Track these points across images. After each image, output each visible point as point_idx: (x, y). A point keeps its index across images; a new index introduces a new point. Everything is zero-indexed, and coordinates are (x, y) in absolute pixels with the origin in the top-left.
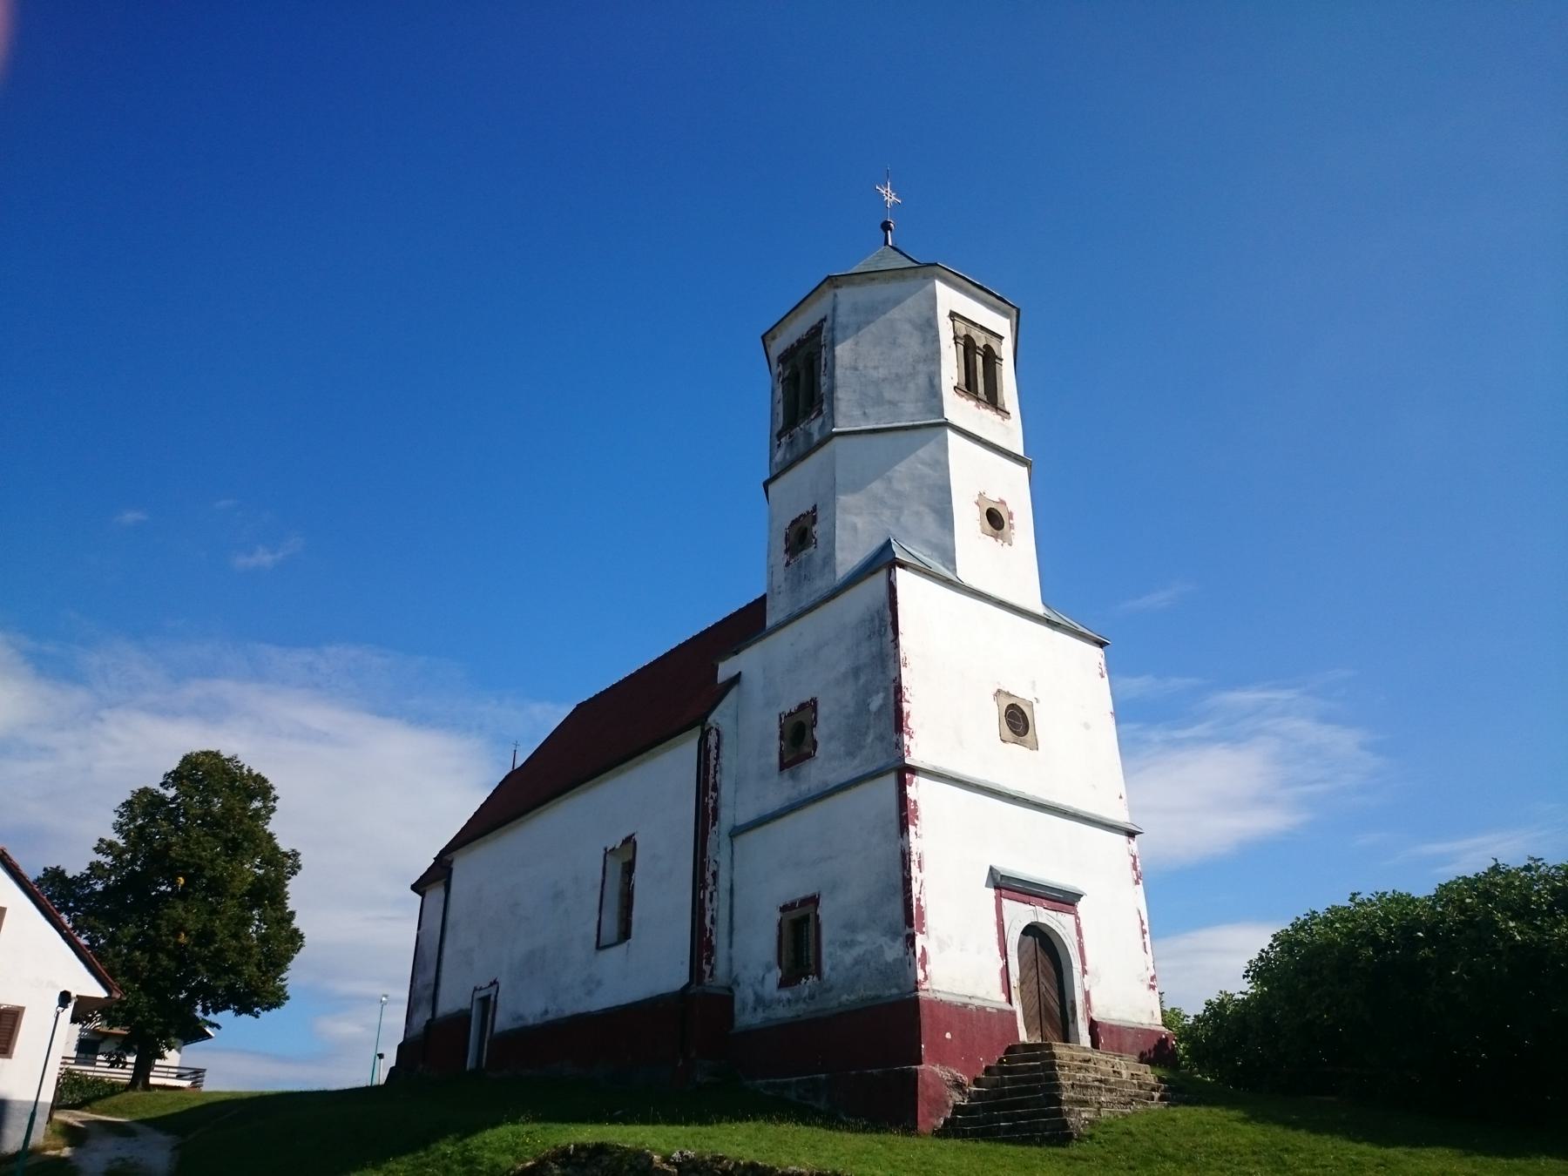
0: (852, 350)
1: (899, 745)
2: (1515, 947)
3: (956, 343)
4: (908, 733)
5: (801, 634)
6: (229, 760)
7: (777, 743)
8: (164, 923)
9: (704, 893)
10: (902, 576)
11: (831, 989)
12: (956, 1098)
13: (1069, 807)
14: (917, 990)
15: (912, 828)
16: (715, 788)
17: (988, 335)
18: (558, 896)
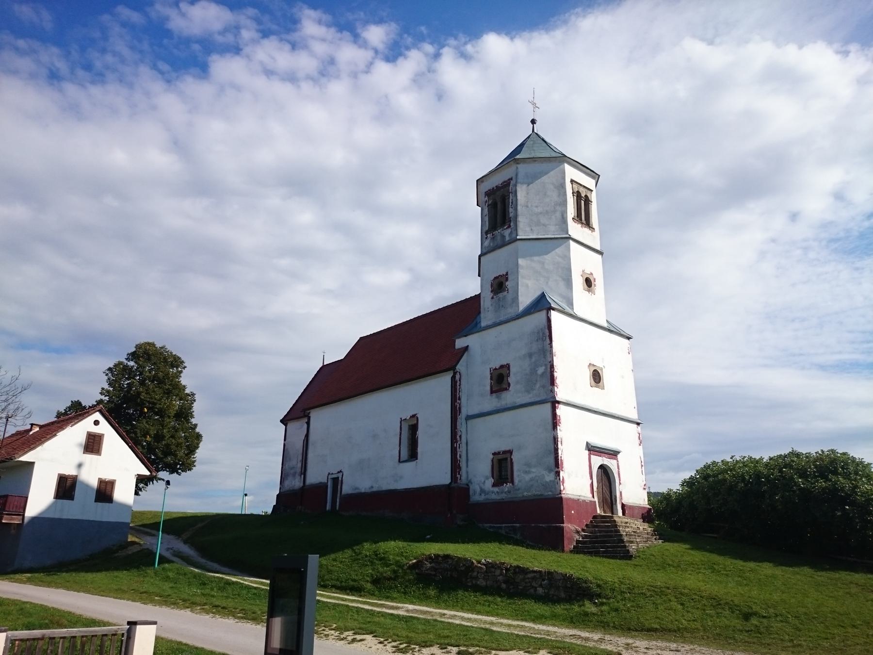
0: (525, 197)
1: (552, 391)
2: (801, 489)
3: (573, 195)
4: (556, 386)
5: (501, 333)
6: (161, 348)
7: (489, 381)
8: (138, 431)
9: (456, 445)
10: (554, 315)
11: (519, 489)
12: (577, 537)
13: (615, 414)
14: (561, 494)
15: (558, 427)
16: (460, 399)
17: (586, 190)
18: (375, 436)
